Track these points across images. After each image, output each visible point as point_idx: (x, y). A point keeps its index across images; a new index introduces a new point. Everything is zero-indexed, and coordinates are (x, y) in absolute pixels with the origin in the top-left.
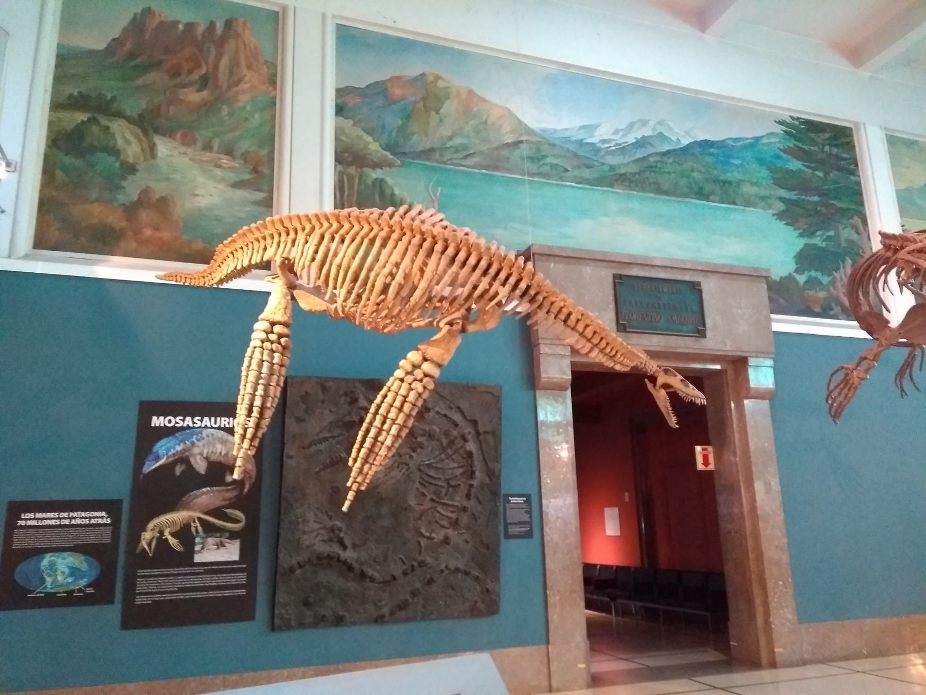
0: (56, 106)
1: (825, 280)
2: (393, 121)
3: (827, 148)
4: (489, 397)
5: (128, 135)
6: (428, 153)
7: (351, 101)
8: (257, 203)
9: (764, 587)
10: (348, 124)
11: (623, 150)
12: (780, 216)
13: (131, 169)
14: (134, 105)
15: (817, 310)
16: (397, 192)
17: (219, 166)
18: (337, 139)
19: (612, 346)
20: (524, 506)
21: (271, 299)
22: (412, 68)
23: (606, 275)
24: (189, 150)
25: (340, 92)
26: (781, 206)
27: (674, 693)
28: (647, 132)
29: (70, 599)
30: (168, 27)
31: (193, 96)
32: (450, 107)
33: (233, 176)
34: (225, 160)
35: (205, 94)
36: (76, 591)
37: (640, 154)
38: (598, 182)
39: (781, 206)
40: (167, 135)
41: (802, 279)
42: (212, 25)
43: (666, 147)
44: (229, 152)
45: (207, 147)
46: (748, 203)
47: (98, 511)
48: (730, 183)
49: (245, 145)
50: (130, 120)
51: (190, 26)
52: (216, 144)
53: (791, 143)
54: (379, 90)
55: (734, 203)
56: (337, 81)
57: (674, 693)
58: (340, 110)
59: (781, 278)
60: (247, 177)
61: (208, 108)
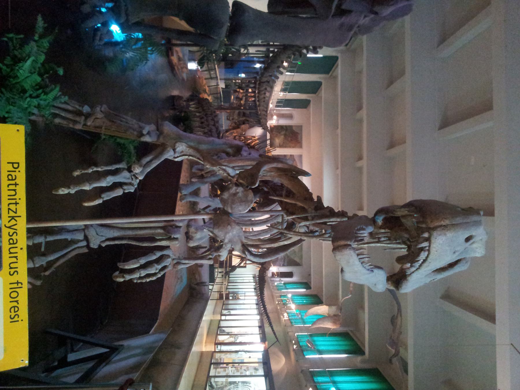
10: (289, 156)
31: (289, 139)
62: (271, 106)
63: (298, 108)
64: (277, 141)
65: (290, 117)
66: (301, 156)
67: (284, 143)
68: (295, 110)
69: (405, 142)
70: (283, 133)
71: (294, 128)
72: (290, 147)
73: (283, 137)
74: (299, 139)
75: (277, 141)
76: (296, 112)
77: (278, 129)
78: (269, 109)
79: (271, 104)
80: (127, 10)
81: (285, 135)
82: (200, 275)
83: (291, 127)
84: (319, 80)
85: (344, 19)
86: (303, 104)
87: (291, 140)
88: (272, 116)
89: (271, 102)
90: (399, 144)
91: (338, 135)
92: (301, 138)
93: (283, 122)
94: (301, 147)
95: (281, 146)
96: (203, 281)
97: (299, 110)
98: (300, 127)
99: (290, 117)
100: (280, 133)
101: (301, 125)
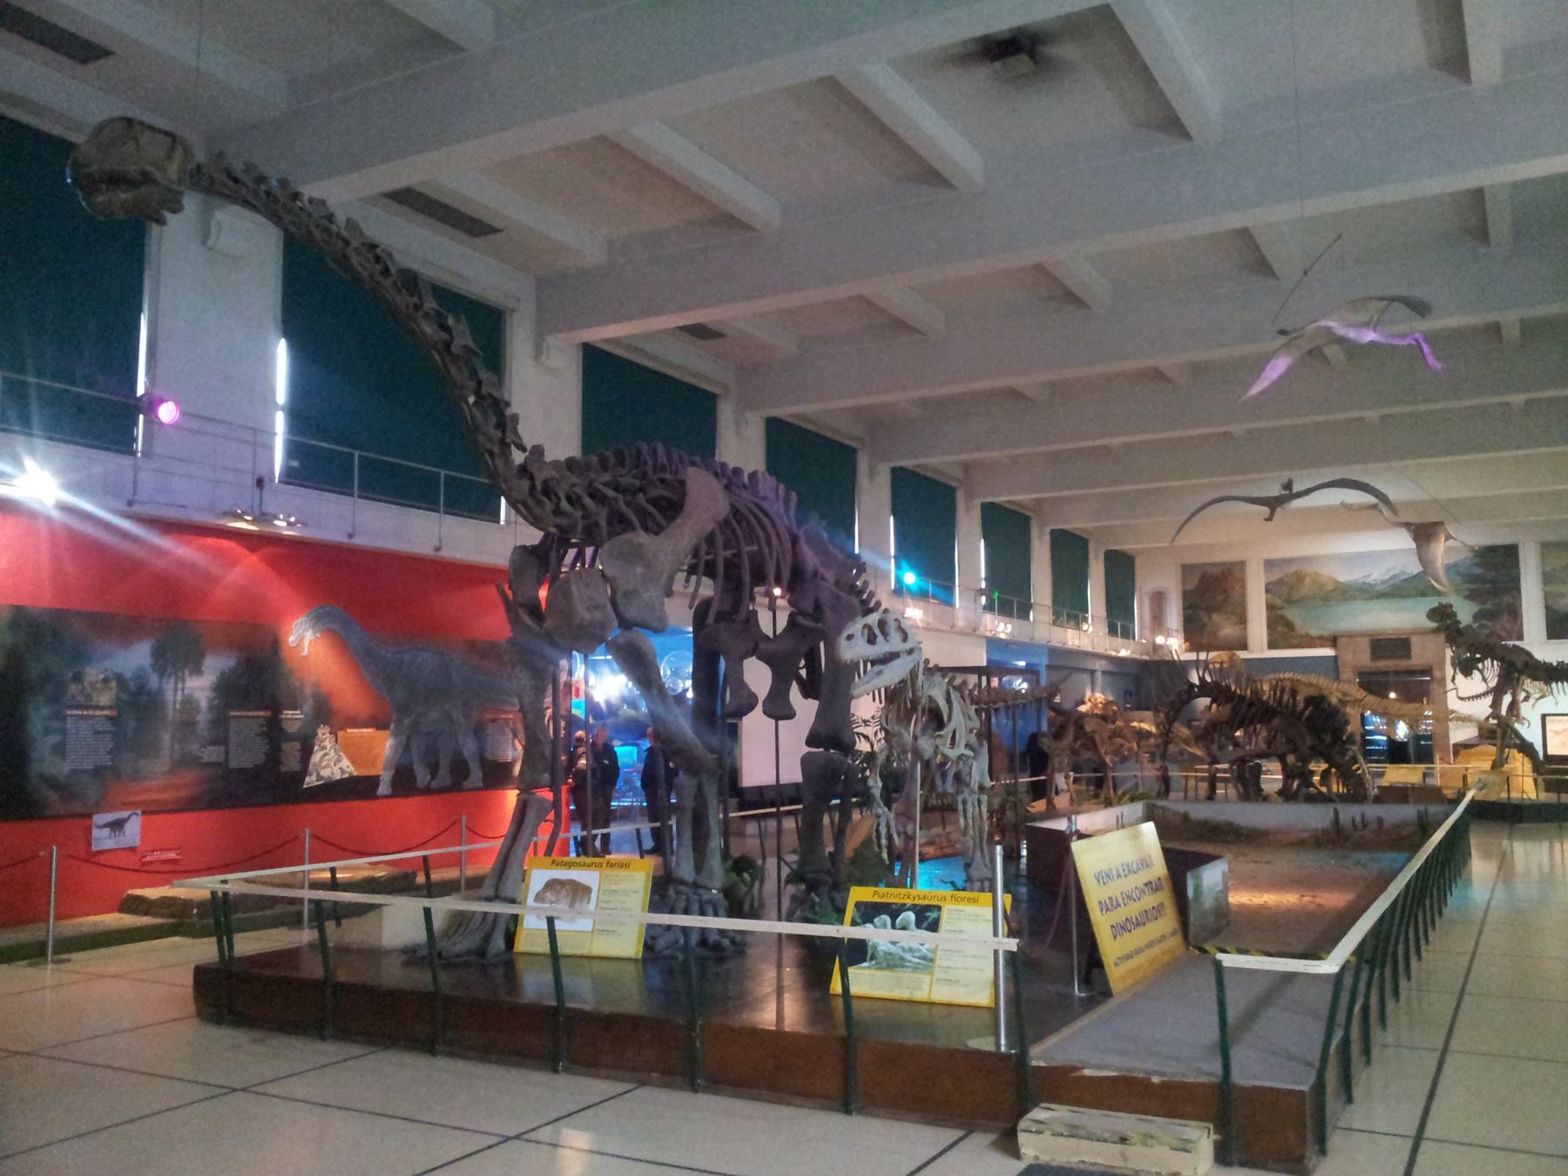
0: (1184, 609)
2: (1285, 590)
6: (1299, 601)
7: (1271, 587)
10: (1269, 596)
11: (1384, 582)
12: (1466, 598)
20: (109, 727)
21: (714, 603)
22: (1292, 569)
23: (1367, 640)
25: (1267, 585)
27: (425, 1173)
28: (1396, 572)
29: (386, 797)
31: (1221, 598)
32: (1307, 581)
37: (1391, 582)
38: (1372, 598)
39: (1467, 593)
40: (295, 464)
41: (1475, 626)
43: (1405, 577)
45: (1226, 613)
53: (1477, 560)
54: (1280, 582)
57: (425, 1173)
58: (1267, 591)
61: (1226, 600)
62: (1124, 653)
63: (1133, 580)
64: (1228, 630)
65: (1158, 599)
66: (1269, 564)
67: (1232, 613)
68: (1140, 589)
69: (1244, 234)
70: (1204, 616)
71: (1190, 586)
72: (1244, 595)
73: (1215, 617)
74: (1218, 570)
75: (1228, 630)
76: (1146, 583)
77: (1195, 633)
78: (1137, 656)
79: (1118, 652)
80: (816, 871)
81: (1210, 610)
82: (1405, 824)
83: (1186, 595)
84: (1047, 539)
85: (826, 609)
86: (1121, 569)
87: (1225, 591)
88: (1156, 648)
89: (1114, 654)
90: (1254, 247)
91: (1250, 432)
92: (1213, 565)
93: (1174, 617)
94: (1242, 565)
95: (1242, 620)
96: (1415, 818)
97: (1137, 577)
98: (1186, 569)
99: (1158, 599)
100: (1205, 625)
101: (1179, 570)
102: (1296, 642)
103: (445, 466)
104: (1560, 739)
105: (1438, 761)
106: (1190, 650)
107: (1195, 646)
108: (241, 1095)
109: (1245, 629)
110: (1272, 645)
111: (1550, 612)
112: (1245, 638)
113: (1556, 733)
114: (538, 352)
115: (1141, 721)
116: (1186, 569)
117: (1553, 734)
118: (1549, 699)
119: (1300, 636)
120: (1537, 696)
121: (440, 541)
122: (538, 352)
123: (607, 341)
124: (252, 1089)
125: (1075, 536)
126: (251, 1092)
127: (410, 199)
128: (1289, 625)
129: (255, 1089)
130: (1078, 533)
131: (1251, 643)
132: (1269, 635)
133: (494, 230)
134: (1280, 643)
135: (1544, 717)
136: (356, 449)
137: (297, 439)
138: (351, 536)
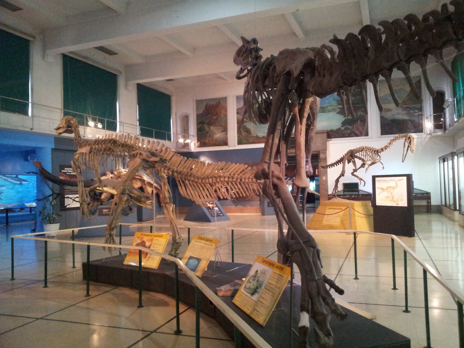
1: (350, 127)
3: (357, 90)
4: (245, 289)
5: (207, 127)
7: (239, 111)
8: (225, 134)
9: (86, 58)
10: (239, 115)
13: (207, 132)
14: (207, 122)
15: (347, 135)
16: (248, 127)
17: (219, 129)
18: (237, 119)
19: (244, 178)
24: (215, 127)
25: (237, 110)
26: (339, 110)
30: (210, 105)
31: (215, 117)
33: (221, 130)
34: (220, 128)
35: (216, 116)
36: (292, 152)
39: (339, 110)
41: (343, 128)
42: (216, 103)
44: (220, 126)
45: (217, 126)
46: (329, 111)
47: (98, 228)
48: (324, 107)
49: (223, 124)
50: (206, 124)
51: (213, 105)
52: (218, 125)
55: (325, 112)
56: (237, 107)
58: (237, 113)
59: (337, 129)
60: (223, 130)
64: (218, 135)
65: (186, 119)
71: (201, 112)
72: (226, 116)
74: (214, 103)
75: (218, 135)
81: (210, 124)
94: (225, 99)
95: (225, 129)
98: (199, 102)
99: (186, 119)
101: (195, 101)
102: (251, 140)
103: (155, 129)
104: (385, 194)
105: (154, 231)
106: (200, 146)
107: (202, 144)
108: (39, 317)
109: (227, 134)
110: (240, 143)
111: (383, 119)
112: (227, 139)
113: (382, 189)
114: (126, 86)
115: (105, 186)
116: (199, 102)
117: (380, 190)
118: (378, 165)
119: (254, 137)
120: (369, 162)
121: (33, 127)
122: (126, 86)
123: (72, 52)
124: (34, 319)
125: (147, 88)
126: (35, 318)
127: (101, 49)
128: (248, 131)
129: (32, 320)
130: (142, 84)
131: (230, 142)
132: (238, 137)
133: (116, 54)
134: (244, 141)
135: (374, 178)
136: (154, 129)
137: (28, 102)
138: (32, 129)
